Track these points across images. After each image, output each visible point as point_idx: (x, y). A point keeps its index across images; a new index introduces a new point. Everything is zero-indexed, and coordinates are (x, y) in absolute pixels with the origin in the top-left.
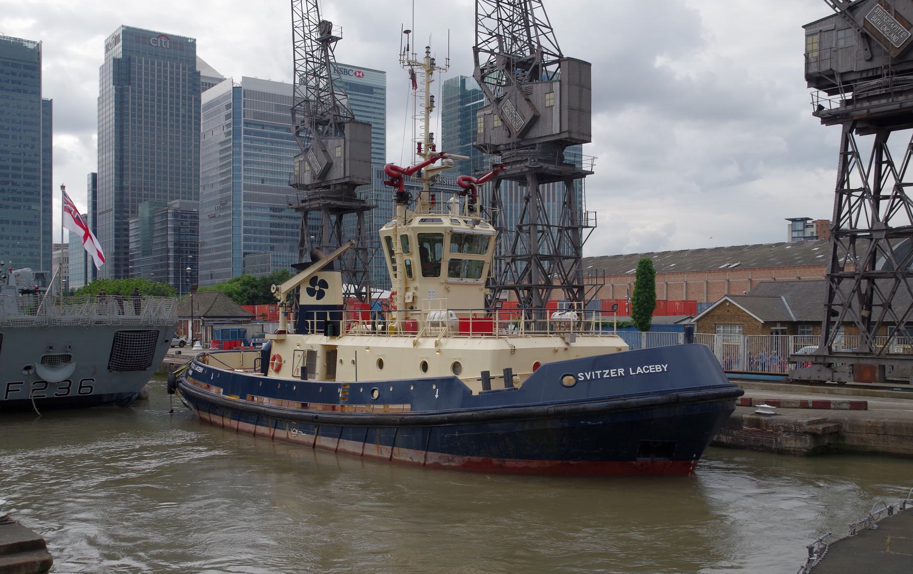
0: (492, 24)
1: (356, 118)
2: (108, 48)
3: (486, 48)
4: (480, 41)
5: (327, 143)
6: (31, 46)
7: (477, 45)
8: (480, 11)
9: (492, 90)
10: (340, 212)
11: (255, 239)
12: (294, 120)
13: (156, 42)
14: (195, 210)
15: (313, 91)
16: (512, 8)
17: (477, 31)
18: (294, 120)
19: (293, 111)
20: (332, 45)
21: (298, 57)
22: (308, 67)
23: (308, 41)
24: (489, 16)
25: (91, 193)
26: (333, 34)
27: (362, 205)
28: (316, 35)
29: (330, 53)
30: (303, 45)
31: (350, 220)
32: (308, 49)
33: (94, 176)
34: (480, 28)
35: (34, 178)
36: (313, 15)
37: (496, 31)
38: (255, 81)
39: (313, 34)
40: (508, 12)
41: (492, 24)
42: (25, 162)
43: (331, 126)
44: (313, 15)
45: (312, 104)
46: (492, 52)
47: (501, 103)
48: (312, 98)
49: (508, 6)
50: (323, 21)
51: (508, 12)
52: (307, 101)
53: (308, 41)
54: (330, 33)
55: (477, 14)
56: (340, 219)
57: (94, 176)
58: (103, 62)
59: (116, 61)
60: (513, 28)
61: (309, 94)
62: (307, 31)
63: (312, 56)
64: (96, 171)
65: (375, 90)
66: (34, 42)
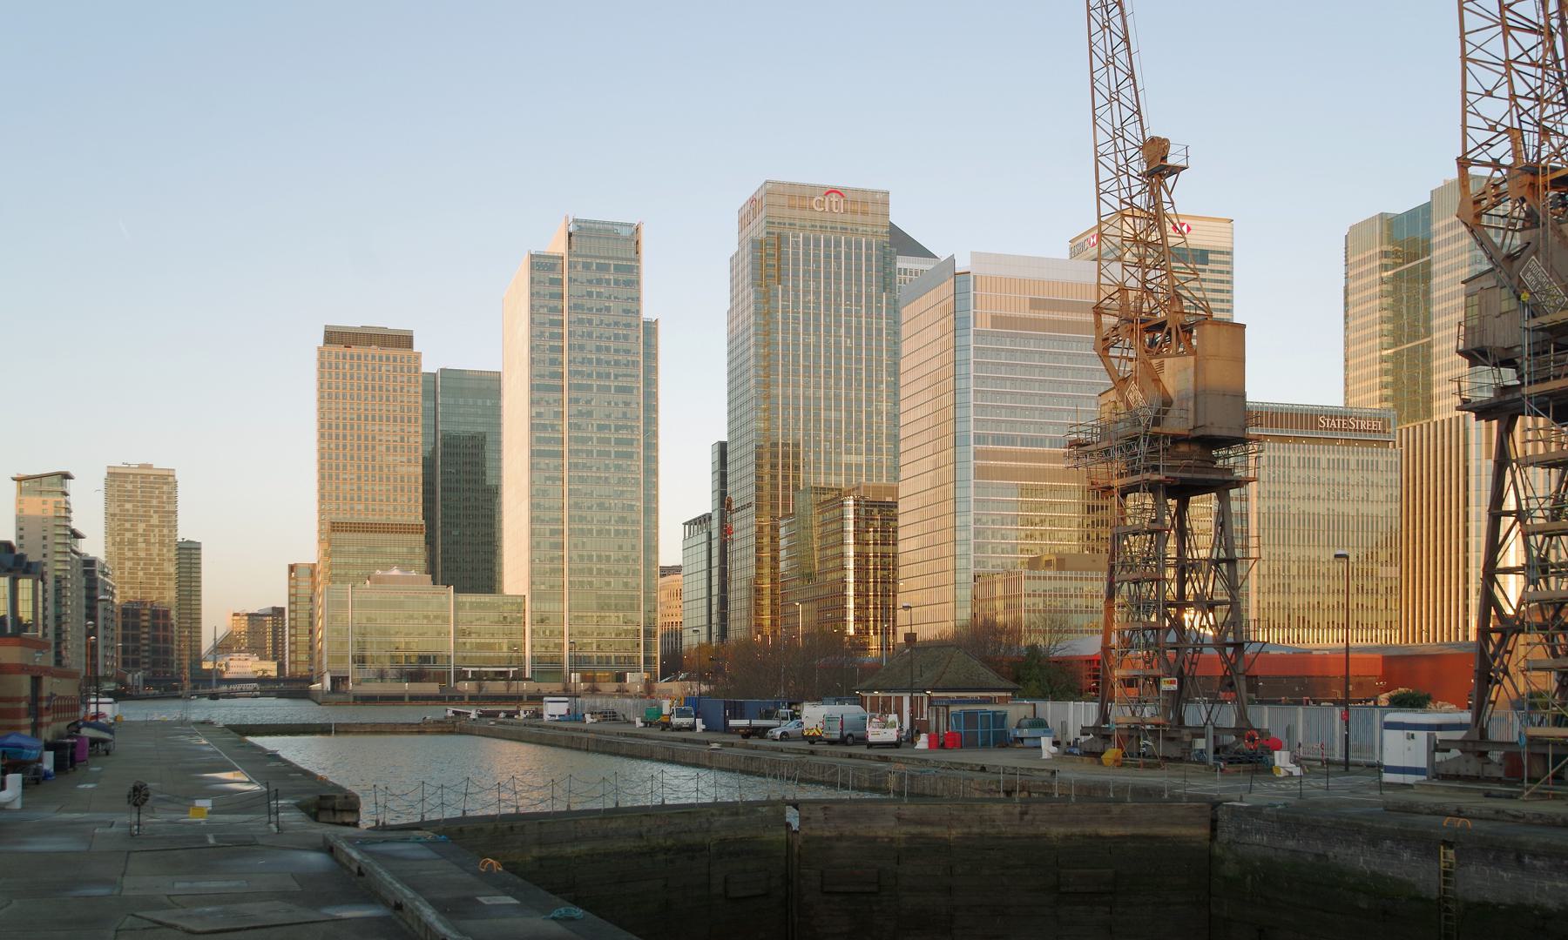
0: (1496, 109)
1: (1216, 315)
2: (744, 222)
3: (1484, 158)
4: (1471, 145)
5: (1161, 365)
6: (625, 232)
7: (1465, 153)
8: (1472, 85)
9: (1498, 241)
10: (1183, 491)
11: (774, 477)
12: (1098, 324)
13: (821, 203)
14: (889, 499)
15: (1133, 270)
16: (1539, 72)
17: (1464, 126)
18: (1098, 324)
19: (1098, 310)
20: (1170, 181)
21: (1105, 209)
22: (1126, 227)
23: (1124, 178)
24: (1489, 94)
25: (717, 476)
26: (1171, 161)
27: (1227, 478)
28: (1138, 166)
29: (1165, 197)
30: (1115, 187)
31: (1202, 509)
32: (1124, 194)
33: (723, 447)
34: (1472, 120)
35: (629, 456)
36: (1132, 129)
37: (1506, 121)
38: (998, 259)
39: (1135, 165)
40: (1531, 81)
41: (1496, 109)
42: (618, 428)
43: (1169, 333)
44: (1132, 129)
45: (1132, 295)
46: (1496, 164)
47: (1517, 264)
48: (1132, 283)
49: (1531, 70)
50: (1153, 139)
51: (1531, 81)
52: (1123, 289)
53: (1124, 178)
54: (1164, 159)
55: (1464, 92)
56: (1183, 506)
57: (723, 447)
58: (736, 248)
59: (757, 245)
60: (1542, 111)
61: (1127, 275)
62: (1121, 161)
63: (1131, 205)
64: (725, 439)
65: (1211, 257)
66: (631, 225)
